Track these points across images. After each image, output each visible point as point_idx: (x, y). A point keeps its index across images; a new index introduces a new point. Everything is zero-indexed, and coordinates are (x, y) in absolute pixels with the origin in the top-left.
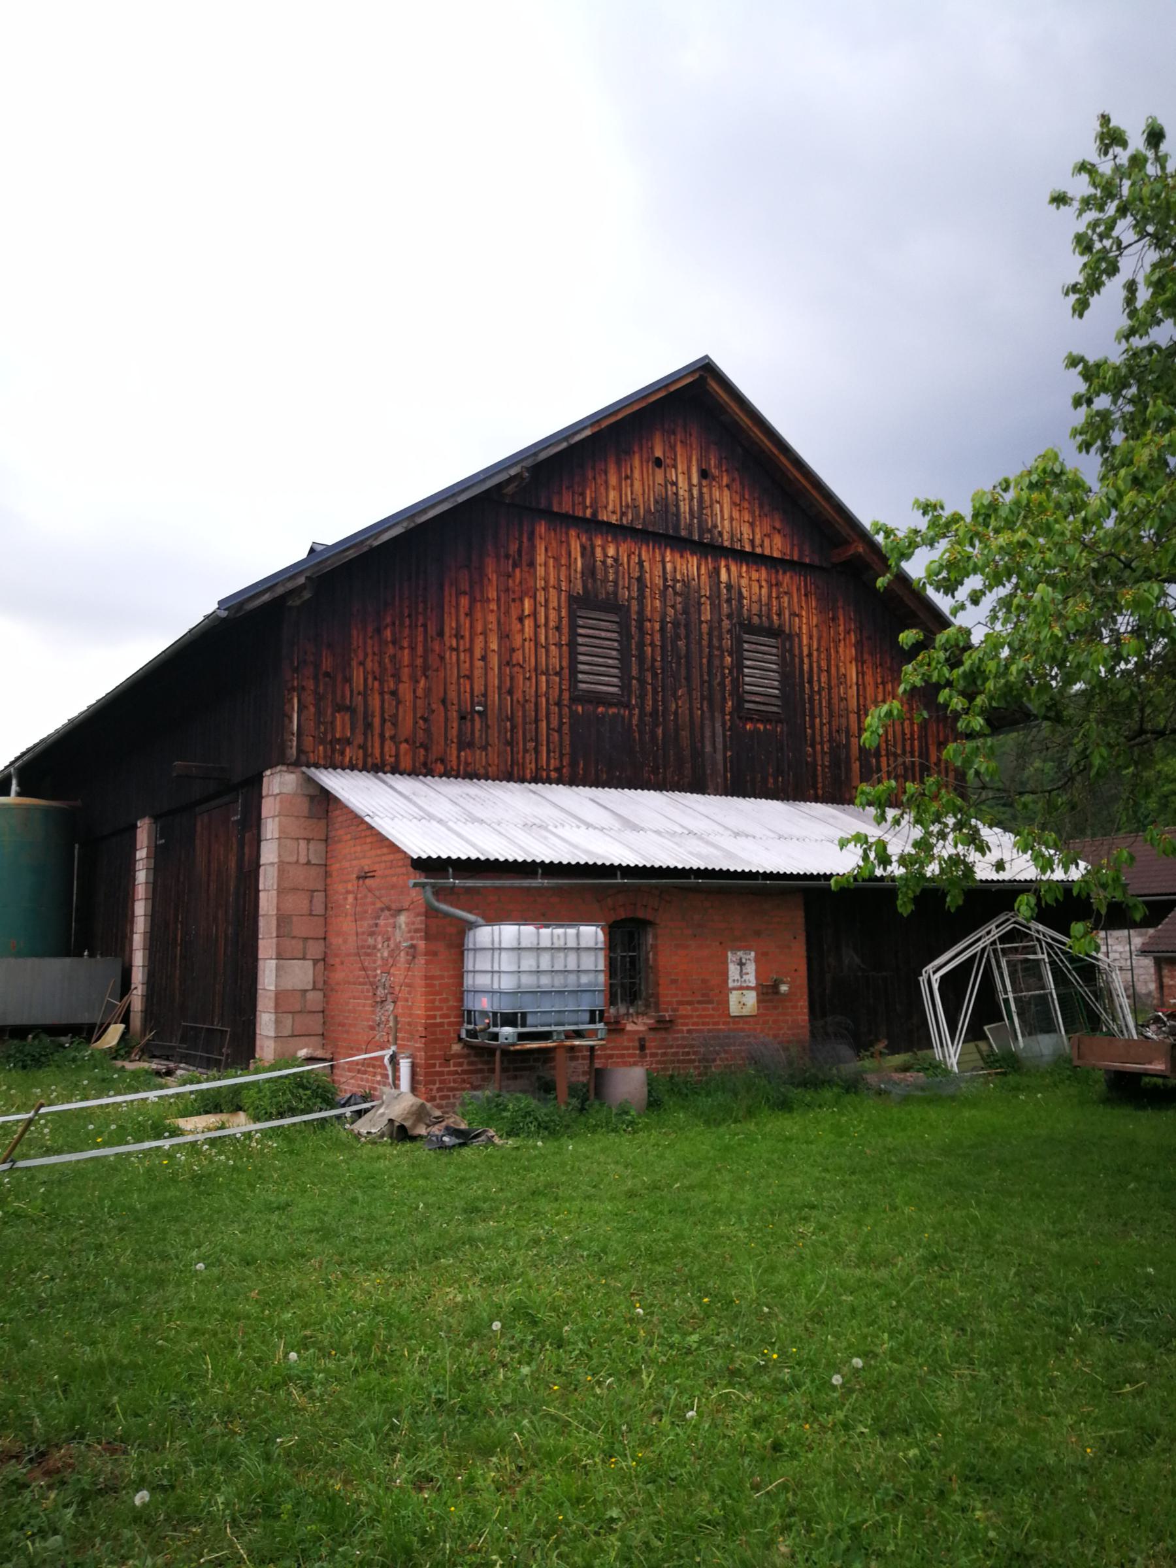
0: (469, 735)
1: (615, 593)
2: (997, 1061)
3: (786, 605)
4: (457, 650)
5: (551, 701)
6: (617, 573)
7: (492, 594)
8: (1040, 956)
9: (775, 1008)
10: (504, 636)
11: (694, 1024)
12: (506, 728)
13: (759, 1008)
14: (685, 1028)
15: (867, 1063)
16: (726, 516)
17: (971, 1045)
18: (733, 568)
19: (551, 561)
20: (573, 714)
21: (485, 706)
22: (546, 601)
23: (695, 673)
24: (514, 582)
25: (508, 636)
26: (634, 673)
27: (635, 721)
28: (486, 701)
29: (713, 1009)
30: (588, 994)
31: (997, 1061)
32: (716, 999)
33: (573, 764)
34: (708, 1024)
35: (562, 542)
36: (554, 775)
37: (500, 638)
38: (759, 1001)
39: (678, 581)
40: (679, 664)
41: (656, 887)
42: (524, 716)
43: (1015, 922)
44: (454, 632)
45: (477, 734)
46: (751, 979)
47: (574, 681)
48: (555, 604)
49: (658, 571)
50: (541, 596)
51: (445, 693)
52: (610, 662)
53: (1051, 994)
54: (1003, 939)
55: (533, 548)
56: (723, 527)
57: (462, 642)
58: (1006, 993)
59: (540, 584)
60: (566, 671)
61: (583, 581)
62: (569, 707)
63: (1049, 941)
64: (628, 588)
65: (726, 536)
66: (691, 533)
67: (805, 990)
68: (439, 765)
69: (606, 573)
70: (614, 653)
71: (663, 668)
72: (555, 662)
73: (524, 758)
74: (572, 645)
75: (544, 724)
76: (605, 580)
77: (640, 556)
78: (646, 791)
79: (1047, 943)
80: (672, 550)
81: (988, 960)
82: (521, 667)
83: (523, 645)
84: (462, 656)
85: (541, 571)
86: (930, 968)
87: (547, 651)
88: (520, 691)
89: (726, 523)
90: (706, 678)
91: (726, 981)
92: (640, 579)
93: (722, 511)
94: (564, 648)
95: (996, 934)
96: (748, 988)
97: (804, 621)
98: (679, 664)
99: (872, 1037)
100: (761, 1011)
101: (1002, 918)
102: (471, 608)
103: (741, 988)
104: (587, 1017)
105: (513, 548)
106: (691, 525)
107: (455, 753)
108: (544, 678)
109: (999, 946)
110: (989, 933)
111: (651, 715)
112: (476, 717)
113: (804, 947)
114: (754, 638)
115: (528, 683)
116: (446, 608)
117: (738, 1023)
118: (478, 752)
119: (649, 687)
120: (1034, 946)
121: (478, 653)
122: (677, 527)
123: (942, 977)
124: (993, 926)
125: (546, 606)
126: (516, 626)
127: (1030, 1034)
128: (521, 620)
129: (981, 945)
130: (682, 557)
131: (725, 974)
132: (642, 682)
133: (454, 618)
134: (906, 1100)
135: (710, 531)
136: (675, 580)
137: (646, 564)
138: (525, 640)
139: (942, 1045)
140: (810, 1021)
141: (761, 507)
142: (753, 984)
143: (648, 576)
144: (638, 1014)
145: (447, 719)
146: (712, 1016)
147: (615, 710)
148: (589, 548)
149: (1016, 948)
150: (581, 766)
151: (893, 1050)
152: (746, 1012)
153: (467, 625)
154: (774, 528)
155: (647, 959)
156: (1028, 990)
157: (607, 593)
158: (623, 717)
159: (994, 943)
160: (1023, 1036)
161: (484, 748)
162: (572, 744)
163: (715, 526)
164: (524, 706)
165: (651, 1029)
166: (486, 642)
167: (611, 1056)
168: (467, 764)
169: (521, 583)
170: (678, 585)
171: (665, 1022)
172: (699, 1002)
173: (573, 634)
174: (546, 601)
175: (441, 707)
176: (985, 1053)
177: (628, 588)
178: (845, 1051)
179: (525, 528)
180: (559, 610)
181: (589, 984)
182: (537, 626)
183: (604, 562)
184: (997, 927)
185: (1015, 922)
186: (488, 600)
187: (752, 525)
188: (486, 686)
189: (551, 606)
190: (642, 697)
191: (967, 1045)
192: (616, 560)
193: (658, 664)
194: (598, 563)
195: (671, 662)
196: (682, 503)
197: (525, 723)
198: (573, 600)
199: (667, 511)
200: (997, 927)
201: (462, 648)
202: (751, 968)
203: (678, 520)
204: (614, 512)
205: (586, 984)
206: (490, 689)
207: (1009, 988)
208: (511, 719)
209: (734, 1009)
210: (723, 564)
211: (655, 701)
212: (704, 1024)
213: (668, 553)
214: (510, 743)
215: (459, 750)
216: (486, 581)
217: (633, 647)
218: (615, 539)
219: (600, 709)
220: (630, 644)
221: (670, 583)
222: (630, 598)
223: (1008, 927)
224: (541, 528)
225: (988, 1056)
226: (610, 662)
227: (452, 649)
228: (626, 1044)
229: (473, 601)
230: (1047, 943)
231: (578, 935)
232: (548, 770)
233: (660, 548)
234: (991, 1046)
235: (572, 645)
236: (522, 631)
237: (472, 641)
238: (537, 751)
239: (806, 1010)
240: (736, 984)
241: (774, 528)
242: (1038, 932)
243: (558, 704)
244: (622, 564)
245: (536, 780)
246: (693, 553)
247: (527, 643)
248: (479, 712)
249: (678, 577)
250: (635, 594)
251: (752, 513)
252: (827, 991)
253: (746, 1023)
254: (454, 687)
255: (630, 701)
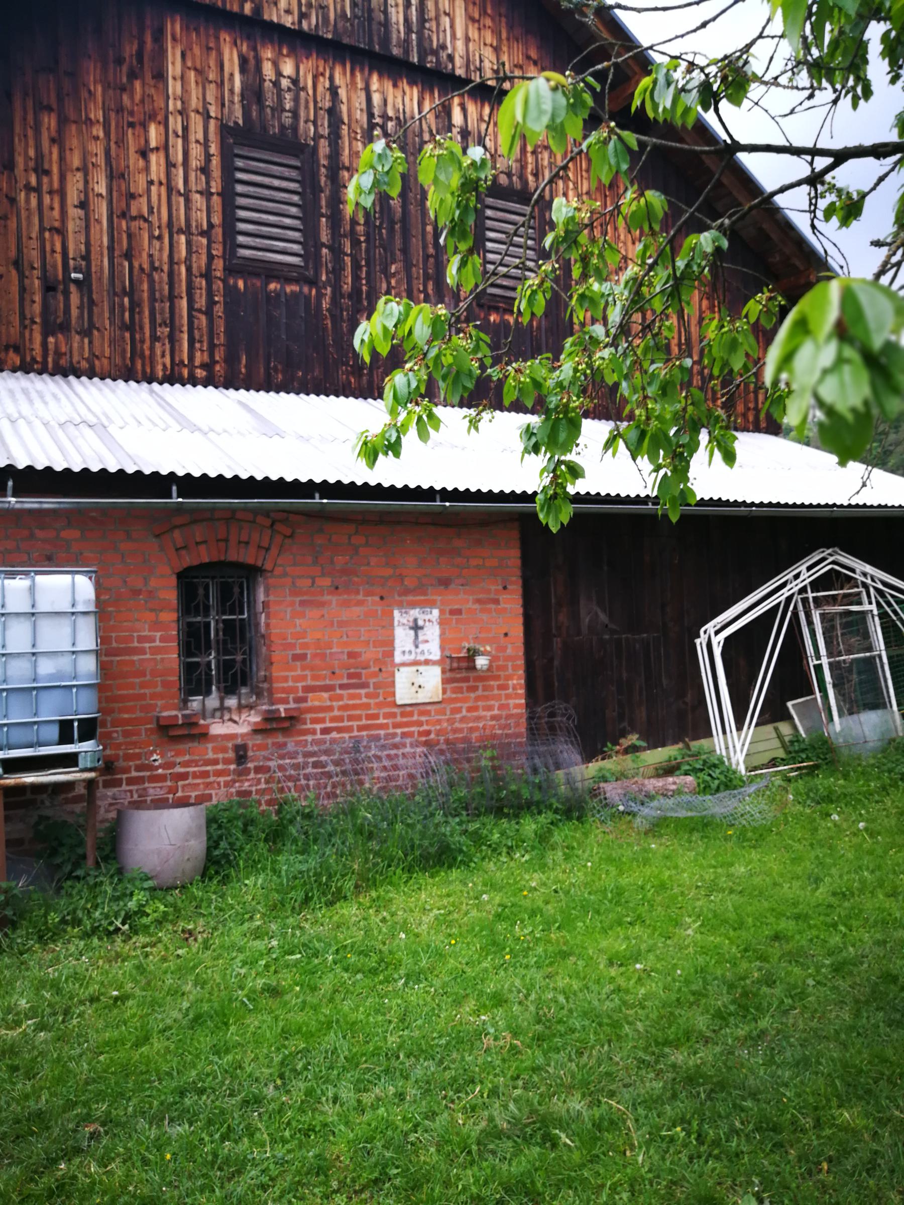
0: (61, 313)
1: (295, 128)
2: (803, 750)
3: (546, 163)
4: (38, 190)
5: (195, 270)
6: (296, 100)
7: (97, 114)
8: (866, 607)
9: (473, 689)
10: (116, 175)
11: (333, 720)
12: (122, 305)
13: (444, 691)
14: (318, 727)
15: (609, 765)
16: (459, 33)
17: (769, 728)
18: (471, 108)
19: (192, 75)
20: (230, 292)
21: (88, 274)
22: (185, 129)
23: (416, 243)
24: (132, 98)
25: (123, 175)
26: (325, 237)
27: (325, 304)
28: (89, 266)
29: (368, 696)
30: (56, 695)
31: (803, 750)
32: (372, 681)
33: (231, 359)
34: (359, 718)
35: (209, 49)
36: (200, 373)
37: (111, 177)
38: (445, 681)
39: (391, 119)
40: (391, 230)
41: (266, 512)
42: (152, 290)
43: (833, 563)
44: (32, 164)
45: (74, 312)
46: (433, 651)
47: (230, 244)
48: (200, 136)
49: (359, 101)
50: (176, 123)
51: (20, 250)
52: (288, 221)
53: (880, 657)
54: (816, 585)
55: (161, 53)
56: (454, 49)
57: (45, 180)
58: (818, 657)
59: (173, 105)
60: (218, 233)
61: (243, 106)
62: (224, 281)
63: (880, 586)
64: (315, 123)
65: (458, 62)
66: (407, 52)
67: (521, 662)
68: (11, 354)
69: (280, 98)
70: (294, 210)
71: (367, 234)
72: (200, 217)
73: (152, 348)
74: (228, 196)
75: (184, 303)
76: (279, 108)
77: (331, 79)
78: (332, 398)
79: (876, 589)
80: (381, 76)
81: (795, 614)
82: (146, 220)
83: (149, 191)
84: (47, 199)
85: (175, 88)
86: (711, 627)
87: (188, 201)
88: (145, 255)
89: (460, 44)
90: (431, 251)
91: (391, 654)
92: (333, 112)
93: (452, 26)
94: (215, 198)
95: (806, 578)
96: (427, 662)
97: (571, 185)
98: (391, 230)
99: (625, 724)
100: (449, 694)
101: (816, 557)
102: (60, 131)
103: (416, 663)
104: (54, 732)
105: (130, 50)
106: (407, 41)
107: (38, 338)
108: (183, 238)
109: (810, 595)
110: (797, 577)
111: (350, 296)
112: (73, 288)
113: (521, 602)
114: (500, 203)
115: (156, 244)
116: (18, 129)
117: (411, 714)
118: (77, 338)
119: (348, 260)
120: (859, 594)
121: (73, 197)
122: (386, 40)
123: (727, 639)
124: (803, 568)
125: (185, 138)
126: (137, 163)
127: (851, 713)
128: (144, 153)
129: (785, 593)
130: (395, 86)
131: (390, 643)
132: (336, 251)
133: (31, 142)
134: (657, 827)
135: (435, 53)
136: (385, 117)
137: (342, 93)
138: (151, 183)
139: (724, 732)
140: (528, 705)
141: (510, 28)
142: (436, 655)
143: (344, 108)
144: (240, 708)
145: (23, 290)
146: (367, 706)
147: (296, 288)
148: (252, 62)
149: (834, 597)
150: (244, 361)
151: (656, 742)
152: (422, 697)
153: (55, 156)
154: (528, 58)
155: (257, 625)
156: (849, 652)
157: (282, 127)
158: (308, 298)
159: (803, 590)
160: (840, 716)
161: (86, 333)
162: (230, 332)
163: (443, 47)
164: (150, 276)
165: (256, 731)
166: (86, 182)
167: (184, 776)
168: (58, 354)
169: (142, 101)
170: (390, 125)
171: (279, 719)
172: (342, 687)
173: (229, 180)
174: (185, 129)
175: (14, 273)
176: (787, 739)
177: (315, 123)
178: (568, 752)
179: (148, 22)
180: (206, 144)
181: (59, 676)
182: (170, 165)
183: (276, 84)
184: (809, 569)
185: (833, 563)
186: (89, 122)
187: (497, 50)
188: (88, 244)
189: (192, 138)
190: (337, 271)
191: (759, 728)
192: (295, 81)
193: (360, 229)
194: (268, 85)
195: (380, 227)
196: (392, 11)
197: (153, 299)
198: (225, 130)
199: (370, 19)
200: (809, 569)
201: (45, 188)
202: (432, 634)
203: (387, 32)
204: (288, 12)
205: (51, 677)
206: (95, 250)
207: (823, 651)
208: (131, 294)
209: (404, 694)
210: (456, 101)
211: (356, 278)
212: (350, 718)
213: (375, 78)
214: (130, 327)
215: (45, 335)
216: (84, 94)
217: (323, 203)
218: (292, 53)
219: (272, 286)
220: (317, 200)
221: (378, 120)
222: (317, 137)
223: (824, 569)
224: (174, 26)
225: (791, 742)
226: (288, 221)
227: (28, 188)
228: (211, 755)
229: (63, 121)
230: (876, 589)
231: (32, 589)
232: (191, 366)
233: (362, 71)
234: (795, 727)
235: (228, 196)
236: (147, 169)
237: (63, 178)
238: (173, 339)
239: (522, 691)
240: (408, 658)
241: (528, 58)
242: (865, 574)
243: (207, 275)
244: (304, 89)
245: (171, 379)
246: (411, 83)
247: (154, 189)
248: (76, 281)
249: (391, 113)
250: (325, 131)
251: (497, 33)
252: (556, 663)
253: (422, 713)
254: (34, 244)
255: (317, 274)
